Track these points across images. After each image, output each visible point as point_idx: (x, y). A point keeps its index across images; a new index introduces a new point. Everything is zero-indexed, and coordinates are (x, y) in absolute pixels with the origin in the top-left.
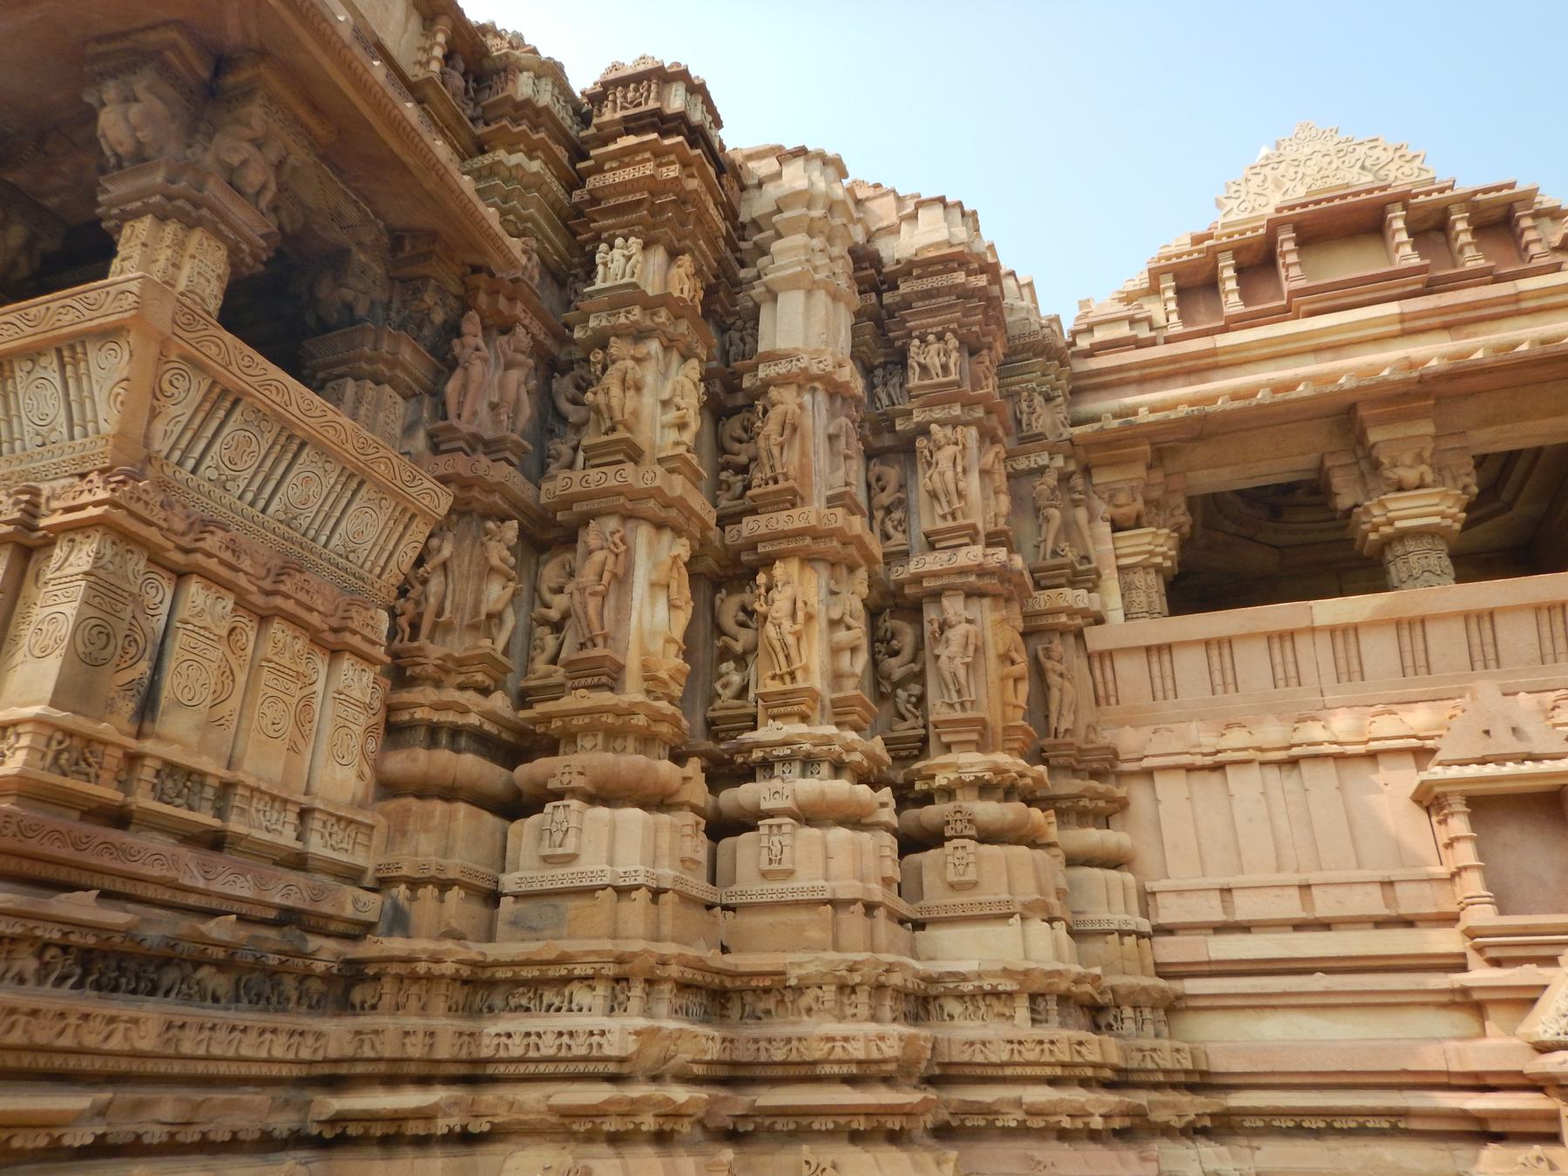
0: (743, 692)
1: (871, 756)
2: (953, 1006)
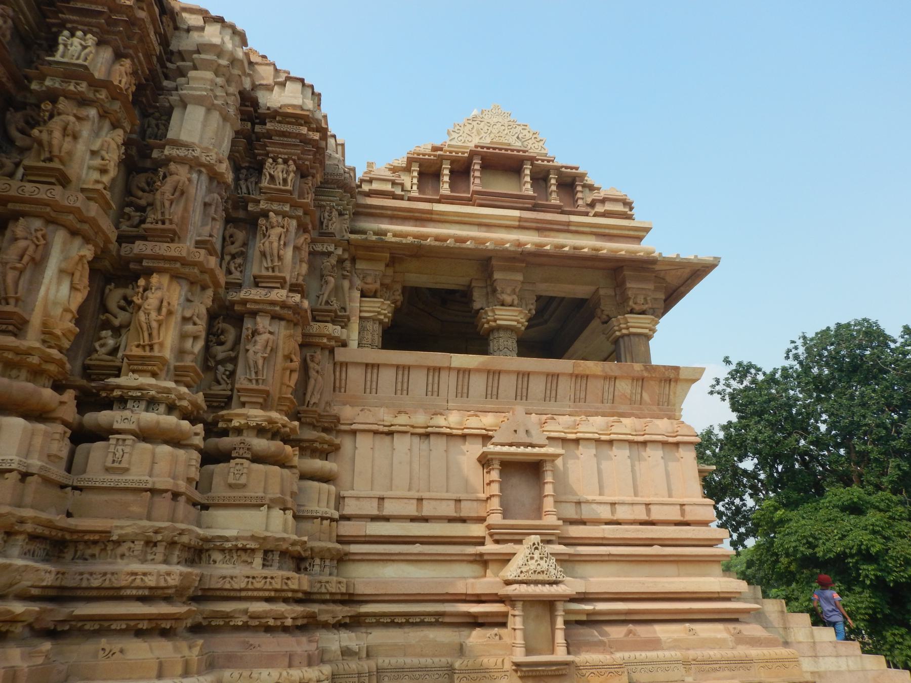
0: (114, 351)
1: (194, 404)
2: (217, 556)
